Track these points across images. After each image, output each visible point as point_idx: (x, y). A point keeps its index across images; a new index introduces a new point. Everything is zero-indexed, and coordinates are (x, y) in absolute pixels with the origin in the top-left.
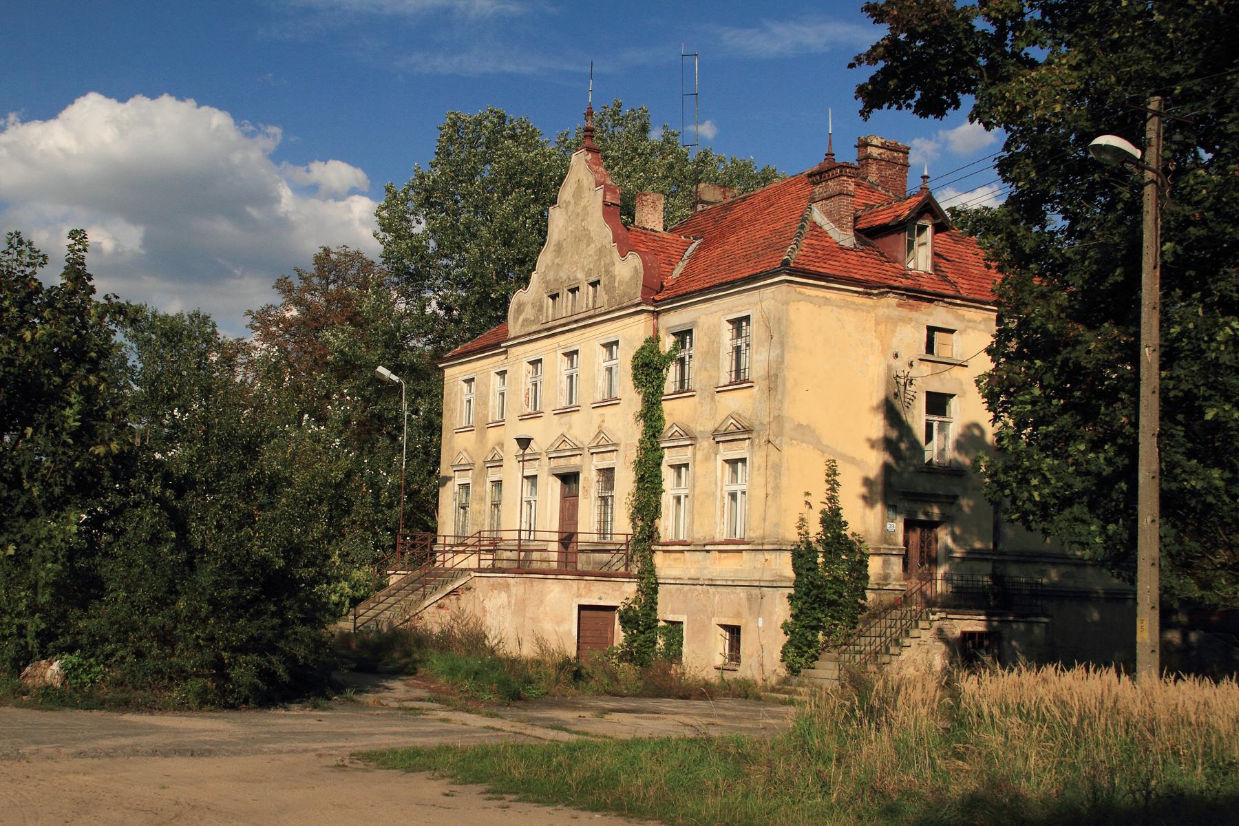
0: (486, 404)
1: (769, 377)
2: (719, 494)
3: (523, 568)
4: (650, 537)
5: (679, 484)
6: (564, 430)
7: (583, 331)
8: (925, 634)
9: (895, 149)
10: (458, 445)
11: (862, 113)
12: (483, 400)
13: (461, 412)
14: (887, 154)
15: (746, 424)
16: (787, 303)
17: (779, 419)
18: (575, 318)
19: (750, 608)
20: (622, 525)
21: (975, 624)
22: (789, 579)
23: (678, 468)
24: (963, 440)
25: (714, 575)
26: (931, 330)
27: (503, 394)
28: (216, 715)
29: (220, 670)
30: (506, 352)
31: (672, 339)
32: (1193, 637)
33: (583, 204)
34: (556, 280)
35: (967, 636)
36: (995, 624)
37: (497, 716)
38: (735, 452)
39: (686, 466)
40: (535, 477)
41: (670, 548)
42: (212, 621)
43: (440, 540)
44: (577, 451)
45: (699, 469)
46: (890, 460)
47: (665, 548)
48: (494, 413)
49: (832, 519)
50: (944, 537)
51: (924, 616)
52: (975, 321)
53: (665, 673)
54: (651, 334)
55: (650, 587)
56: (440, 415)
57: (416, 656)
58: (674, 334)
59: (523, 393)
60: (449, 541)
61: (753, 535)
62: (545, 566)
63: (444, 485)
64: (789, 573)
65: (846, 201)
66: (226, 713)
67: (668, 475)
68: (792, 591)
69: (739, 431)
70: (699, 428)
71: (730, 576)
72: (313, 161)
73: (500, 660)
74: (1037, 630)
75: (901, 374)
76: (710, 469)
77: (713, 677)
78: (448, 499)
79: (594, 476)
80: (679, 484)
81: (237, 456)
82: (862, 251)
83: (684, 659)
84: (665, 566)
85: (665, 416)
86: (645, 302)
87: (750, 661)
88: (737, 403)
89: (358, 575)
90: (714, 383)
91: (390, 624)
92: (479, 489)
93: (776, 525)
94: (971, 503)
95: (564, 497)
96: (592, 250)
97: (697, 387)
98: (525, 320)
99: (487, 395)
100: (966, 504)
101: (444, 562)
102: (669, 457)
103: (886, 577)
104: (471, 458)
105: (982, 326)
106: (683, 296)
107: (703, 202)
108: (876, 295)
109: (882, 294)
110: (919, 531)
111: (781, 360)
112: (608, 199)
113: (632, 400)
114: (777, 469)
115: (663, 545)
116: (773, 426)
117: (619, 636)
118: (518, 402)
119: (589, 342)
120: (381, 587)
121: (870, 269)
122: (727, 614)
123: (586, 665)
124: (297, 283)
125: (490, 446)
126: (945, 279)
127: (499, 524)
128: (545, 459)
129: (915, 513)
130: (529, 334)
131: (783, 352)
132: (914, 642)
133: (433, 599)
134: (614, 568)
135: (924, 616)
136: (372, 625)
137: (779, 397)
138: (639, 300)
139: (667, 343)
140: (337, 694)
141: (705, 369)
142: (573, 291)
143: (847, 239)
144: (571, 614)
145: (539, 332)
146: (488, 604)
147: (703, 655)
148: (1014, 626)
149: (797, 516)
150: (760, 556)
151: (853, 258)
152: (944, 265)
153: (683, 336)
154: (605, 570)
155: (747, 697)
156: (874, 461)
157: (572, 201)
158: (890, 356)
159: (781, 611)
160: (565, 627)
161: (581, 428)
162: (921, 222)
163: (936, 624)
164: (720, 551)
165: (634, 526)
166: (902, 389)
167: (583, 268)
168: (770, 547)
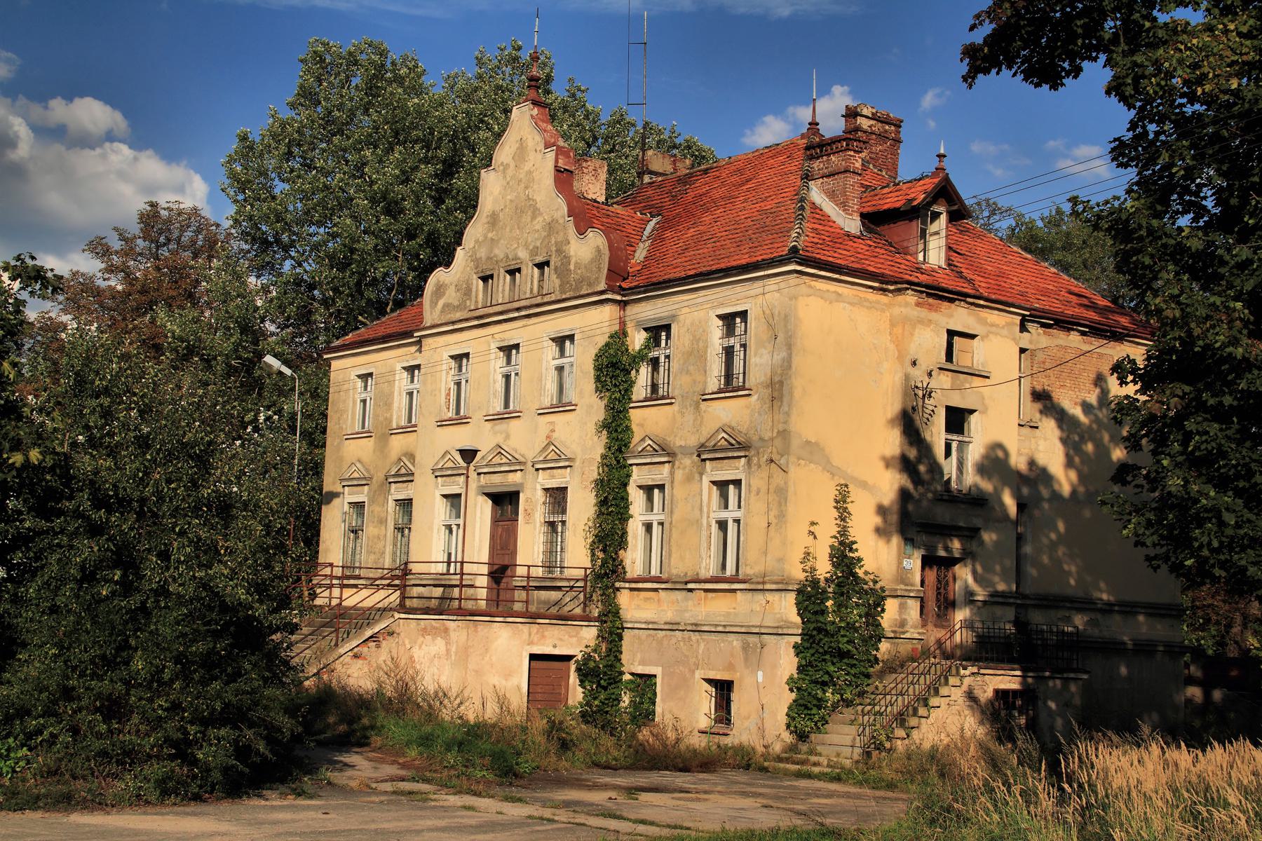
0: (389, 405)
1: (771, 384)
2: (705, 522)
3: (442, 608)
4: (614, 572)
6: (499, 439)
7: (525, 322)
8: (954, 693)
9: (885, 121)
10: (347, 454)
11: (965, 79)
14: (878, 127)
16: (794, 298)
17: (784, 434)
18: (516, 305)
19: (746, 659)
20: (578, 555)
21: (1009, 680)
22: (797, 626)
23: (648, 490)
24: (986, 463)
26: (951, 334)
27: (411, 394)
28: (188, 809)
29: (182, 750)
30: (419, 343)
31: (644, 335)
32: (1217, 695)
33: (526, 168)
34: (489, 258)
35: (1001, 694)
36: (1030, 680)
37: (520, 800)
39: (661, 487)
41: (640, 585)
42: (177, 685)
44: (517, 464)
45: (678, 491)
46: (910, 486)
47: (633, 585)
48: (399, 417)
49: (844, 556)
50: (964, 575)
51: (954, 671)
52: (997, 326)
54: (617, 328)
55: (612, 630)
57: (365, 721)
58: (646, 329)
63: (329, 502)
65: (852, 180)
66: (193, 807)
67: (636, 498)
68: (798, 639)
72: (53, 97)
74: (1073, 688)
75: (920, 385)
76: (695, 496)
77: (698, 742)
79: (540, 496)
81: (188, 468)
82: (870, 239)
84: (632, 606)
85: (634, 427)
86: (610, 289)
87: (746, 724)
88: (729, 413)
90: (699, 388)
92: (377, 509)
93: (780, 560)
94: (994, 537)
95: (495, 521)
96: (539, 224)
98: (446, 306)
99: (392, 394)
100: (988, 537)
102: (638, 476)
103: (902, 624)
104: (367, 470)
105: (1005, 332)
106: (658, 286)
107: (651, 173)
109: (899, 290)
110: (935, 569)
111: (787, 364)
113: (590, 406)
114: (781, 494)
116: (778, 442)
117: (576, 694)
119: (534, 334)
121: (881, 262)
122: (721, 665)
124: (116, 245)
126: (960, 275)
129: (935, 548)
130: (453, 323)
131: (790, 356)
132: (943, 702)
134: (567, 609)
135: (954, 671)
138: (602, 286)
139: (637, 340)
140: (305, 774)
141: (688, 372)
142: (512, 272)
143: (853, 225)
144: (520, 665)
145: (467, 320)
147: (685, 713)
148: (1051, 684)
149: (803, 548)
150: (759, 597)
151: (861, 246)
152: (957, 260)
153: (658, 332)
154: (554, 610)
155: (747, 767)
156: (888, 484)
157: (512, 165)
158: (908, 363)
159: (788, 664)
160: (514, 681)
161: (523, 438)
162: (936, 208)
163: (967, 681)
166: (920, 404)
167: (526, 246)
168: (774, 587)
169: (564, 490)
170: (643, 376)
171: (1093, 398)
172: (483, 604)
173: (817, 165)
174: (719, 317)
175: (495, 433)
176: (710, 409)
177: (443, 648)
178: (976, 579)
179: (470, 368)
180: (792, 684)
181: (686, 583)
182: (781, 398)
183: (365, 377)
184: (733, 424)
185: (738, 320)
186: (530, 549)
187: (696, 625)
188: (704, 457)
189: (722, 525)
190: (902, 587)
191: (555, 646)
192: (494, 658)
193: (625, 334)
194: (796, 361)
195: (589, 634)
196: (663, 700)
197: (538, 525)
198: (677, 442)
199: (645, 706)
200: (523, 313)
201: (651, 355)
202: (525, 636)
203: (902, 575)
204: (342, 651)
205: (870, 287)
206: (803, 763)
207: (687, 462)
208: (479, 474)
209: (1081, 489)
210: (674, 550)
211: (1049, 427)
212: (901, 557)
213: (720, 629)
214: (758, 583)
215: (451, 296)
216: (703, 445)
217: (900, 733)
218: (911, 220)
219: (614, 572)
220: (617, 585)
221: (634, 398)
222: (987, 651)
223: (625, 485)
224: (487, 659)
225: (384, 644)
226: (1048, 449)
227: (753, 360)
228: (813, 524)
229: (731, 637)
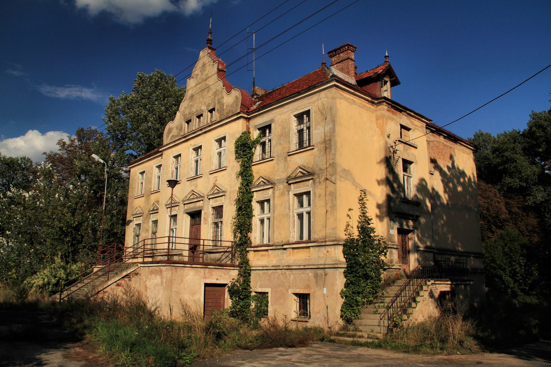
1: (325, 141)
3: (170, 259)
4: (246, 243)
10: (136, 204)
12: (149, 181)
13: (138, 188)
17: (333, 165)
19: (317, 282)
20: (228, 235)
21: (444, 286)
23: (261, 203)
24: (419, 187)
27: (159, 177)
30: (162, 155)
33: (206, 73)
34: (190, 113)
38: (301, 188)
39: (268, 201)
40: (176, 215)
41: (259, 249)
44: (200, 198)
45: (277, 202)
47: (255, 249)
48: (154, 187)
55: (246, 271)
57: (86, 322)
58: (259, 129)
59: (171, 173)
63: (128, 225)
64: (342, 258)
65: (351, 63)
67: (256, 207)
70: (277, 178)
78: (130, 231)
79: (211, 211)
84: (255, 259)
85: (254, 174)
87: (318, 316)
88: (303, 159)
90: (287, 150)
92: (145, 225)
95: (192, 225)
98: (173, 136)
100: (422, 220)
102: (257, 197)
104: (142, 210)
105: (421, 129)
108: (376, 104)
111: (333, 130)
112: (220, 67)
113: (234, 166)
114: (333, 195)
115: (253, 247)
116: (330, 170)
117: (228, 302)
119: (208, 141)
125: (152, 203)
128: (181, 205)
130: (174, 142)
131: (334, 126)
133: (113, 280)
137: (333, 152)
138: (239, 111)
142: (199, 117)
144: (200, 289)
146: (148, 283)
147: (283, 311)
149: (344, 223)
150: (323, 249)
153: (265, 129)
158: (386, 136)
161: (203, 186)
164: (293, 248)
165: (235, 237)
167: (205, 104)
168: (331, 243)
169: (221, 207)
170: (258, 151)
171: (450, 165)
172: (186, 259)
173: (333, 59)
174: (295, 116)
175: (191, 186)
176: (292, 159)
177: (160, 280)
178: (418, 239)
179: (182, 160)
180: (343, 294)
181: (283, 245)
182: (330, 148)
183: (142, 173)
184: (305, 164)
185: (305, 116)
186: (207, 232)
187: (289, 266)
188: (289, 182)
189: (300, 216)
190: (390, 243)
191: (217, 279)
192: (186, 286)
193: (249, 133)
194: (337, 128)
195: (234, 273)
196: (272, 305)
197: (210, 224)
198: (275, 178)
199: (263, 308)
200: (203, 131)
201: (262, 141)
202: (202, 274)
203: (390, 237)
204: (110, 283)
205: (367, 100)
206: (353, 336)
207: (281, 186)
208: (184, 204)
209: (450, 203)
210: (275, 230)
211: (437, 173)
212: (389, 228)
213: (302, 267)
214: (322, 242)
215: (175, 132)
216: (289, 177)
217: (405, 317)
218: (376, 82)
219: (246, 243)
220: (248, 249)
221: (254, 161)
222: (426, 273)
223: (250, 201)
224: (182, 286)
225: (133, 279)
226: (436, 183)
227: (314, 132)
228: (350, 210)
229: (308, 271)
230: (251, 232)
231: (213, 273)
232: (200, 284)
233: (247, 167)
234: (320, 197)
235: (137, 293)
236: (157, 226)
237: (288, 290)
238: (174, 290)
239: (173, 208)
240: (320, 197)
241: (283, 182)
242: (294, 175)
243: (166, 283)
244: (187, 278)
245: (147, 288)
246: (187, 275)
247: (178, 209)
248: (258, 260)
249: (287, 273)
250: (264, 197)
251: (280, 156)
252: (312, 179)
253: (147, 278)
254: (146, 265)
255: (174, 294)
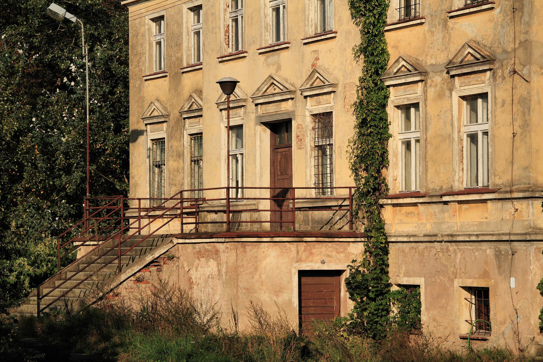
0: (179, 45)
2: (456, 136)
3: (232, 228)
4: (375, 190)
5: (408, 127)
6: (271, 71)
10: (148, 94)
12: (176, 42)
13: (151, 55)
15: (486, 53)
17: (526, 44)
19: (499, 267)
20: (344, 177)
23: (406, 108)
25: (455, 229)
27: (198, 33)
39: (416, 106)
40: (240, 127)
41: (401, 201)
43: (134, 204)
44: (288, 94)
45: (431, 108)
47: (395, 201)
48: (188, 56)
53: (402, 345)
56: (125, 63)
57: (116, 339)
59: (223, 31)
60: (146, 204)
61: (498, 181)
62: (256, 227)
63: (135, 140)
67: (395, 117)
69: (478, 62)
71: (474, 230)
73: (214, 339)
78: (140, 156)
79: (309, 122)
80: (408, 127)
83: (424, 330)
84: (397, 222)
85: (390, 50)
87: (503, 329)
89: (41, 249)
90: (446, 6)
91: (82, 303)
92: (175, 144)
93: (526, 168)
95: (274, 149)
97: (426, 13)
99: (181, 34)
101: (140, 229)
102: (396, 96)
104: (165, 108)
114: (525, 103)
115: (392, 198)
116: (520, 53)
117: (348, 306)
118: (217, 42)
120: (67, 261)
123: (313, 340)
125: (186, 92)
127: (201, 183)
128: (251, 106)
133: (130, 272)
136: (60, 305)
137: (526, 18)
144: (290, 282)
146: (194, 274)
150: (508, 205)
154: (326, 229)
161: (291, 68)
164: (460, 202)
165: (357, 178)
168: (521, 195)
169: (329, 115)
175: (268, 65)
176: (457, 26)
177: (215, 269)
181: (441, 196)
184: (479, 39)
187: (452, 236)
188: (452, 73)
191: (323, 262)
192: (263, 277)
196: (427, 309)
197: (309, 149)
202: (293, 253)
208: (257, 105)
213: (473, 238)
214: (506, 192)
216: (450, 62)
221: (389, 21)
224: (256, 277)
229: (485, 246)
230: (387, 168)
231: (314, 251)
232: (290, 273)
233: (376, 36)
234: (503, 106)
235: (177, 293)
236: (200, 145)
237: (453, 281)
238: (240, 284)
239: (231, 111)
240: (503, 106)
241: (442, 71)
242: (460, 59)
243: (226, 273)
244: (264, 263)
245: (192, 283)
246: (265, 258)
247: (245, 113)
248: (401, 222)
249: (451, 248)
250: (408, 99)
251: (436, 16)
252: (490, 70)
253: (191, 265)
254: (187, 241)
255: (252, 286)
